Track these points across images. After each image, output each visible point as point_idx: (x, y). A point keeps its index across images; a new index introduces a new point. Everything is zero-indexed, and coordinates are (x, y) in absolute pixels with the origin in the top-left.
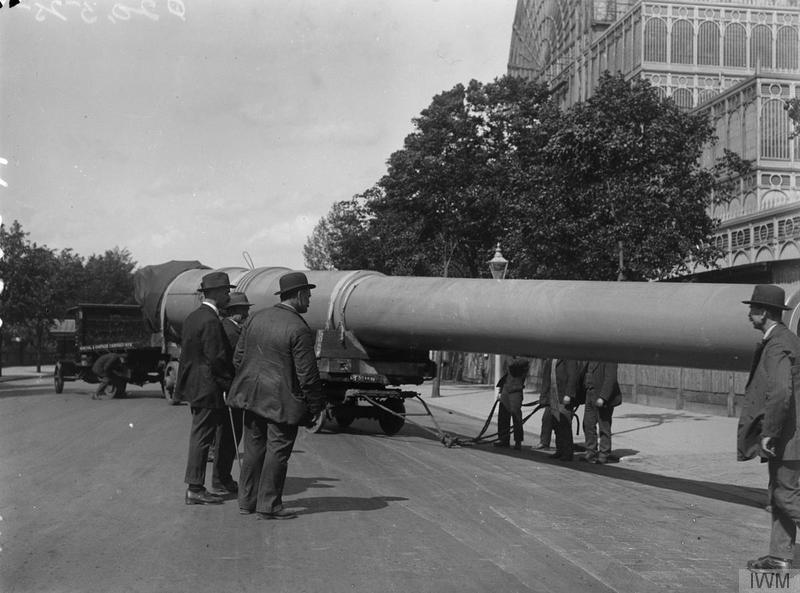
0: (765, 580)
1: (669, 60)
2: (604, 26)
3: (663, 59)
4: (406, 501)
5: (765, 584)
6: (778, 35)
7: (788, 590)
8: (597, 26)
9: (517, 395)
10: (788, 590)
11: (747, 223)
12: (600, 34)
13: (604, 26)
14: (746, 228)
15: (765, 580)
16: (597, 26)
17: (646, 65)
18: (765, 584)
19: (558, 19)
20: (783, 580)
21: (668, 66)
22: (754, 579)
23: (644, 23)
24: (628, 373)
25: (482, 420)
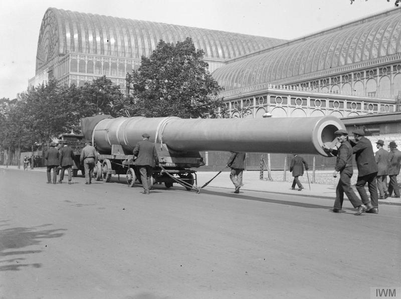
0: (383, 293)
1: (78, 71)
2: (64, 55)
3: (76, 71)
4: (51, 226)
5: (383, 294)
6: (80, 83)
7: (395, 298)
8: (60, 55)
9: (296, 175)
10: (395, 298)
11: (252, 96)
12: (61, 58)
13: (63, 55)
14: (252, 98)
15: (383, 293)
16: (60, 55)
17: (71, 73)
18: (383, 294)
19: (50, 46)
20: (392, 292)
21: (78, 73)
22: (378, 292)
23: (70, 60)
24: (206, 155)
25: (332, 207)
